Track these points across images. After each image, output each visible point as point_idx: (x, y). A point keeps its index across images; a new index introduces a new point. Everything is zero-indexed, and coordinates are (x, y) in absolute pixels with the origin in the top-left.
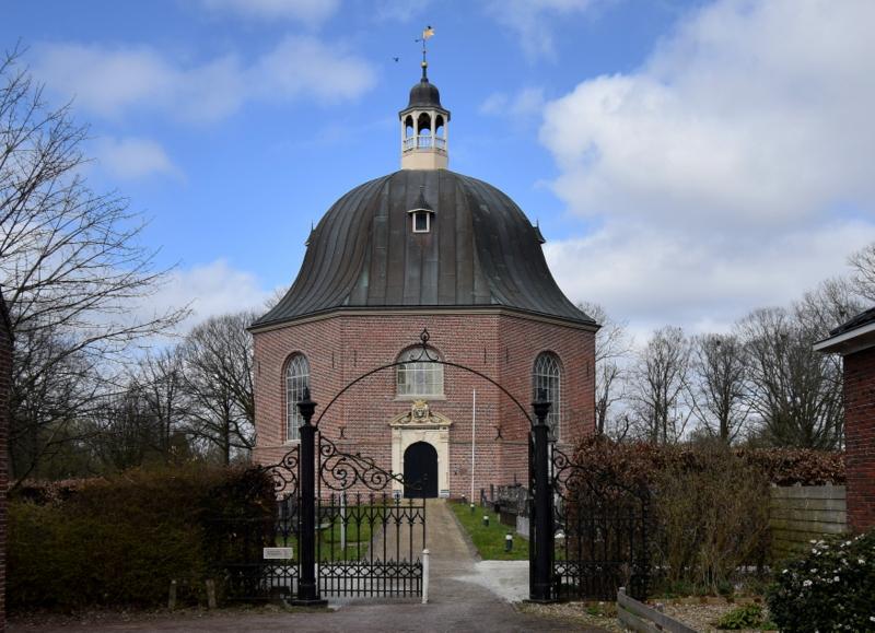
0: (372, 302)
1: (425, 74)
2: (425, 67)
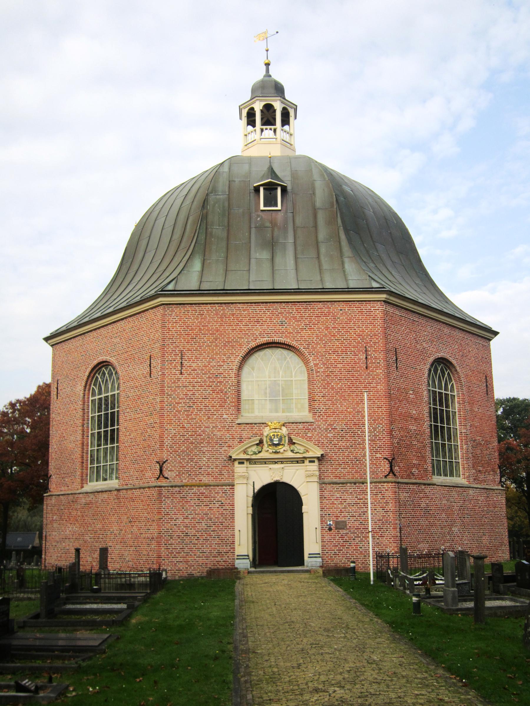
1: (268, 70)
2: (267, 65)
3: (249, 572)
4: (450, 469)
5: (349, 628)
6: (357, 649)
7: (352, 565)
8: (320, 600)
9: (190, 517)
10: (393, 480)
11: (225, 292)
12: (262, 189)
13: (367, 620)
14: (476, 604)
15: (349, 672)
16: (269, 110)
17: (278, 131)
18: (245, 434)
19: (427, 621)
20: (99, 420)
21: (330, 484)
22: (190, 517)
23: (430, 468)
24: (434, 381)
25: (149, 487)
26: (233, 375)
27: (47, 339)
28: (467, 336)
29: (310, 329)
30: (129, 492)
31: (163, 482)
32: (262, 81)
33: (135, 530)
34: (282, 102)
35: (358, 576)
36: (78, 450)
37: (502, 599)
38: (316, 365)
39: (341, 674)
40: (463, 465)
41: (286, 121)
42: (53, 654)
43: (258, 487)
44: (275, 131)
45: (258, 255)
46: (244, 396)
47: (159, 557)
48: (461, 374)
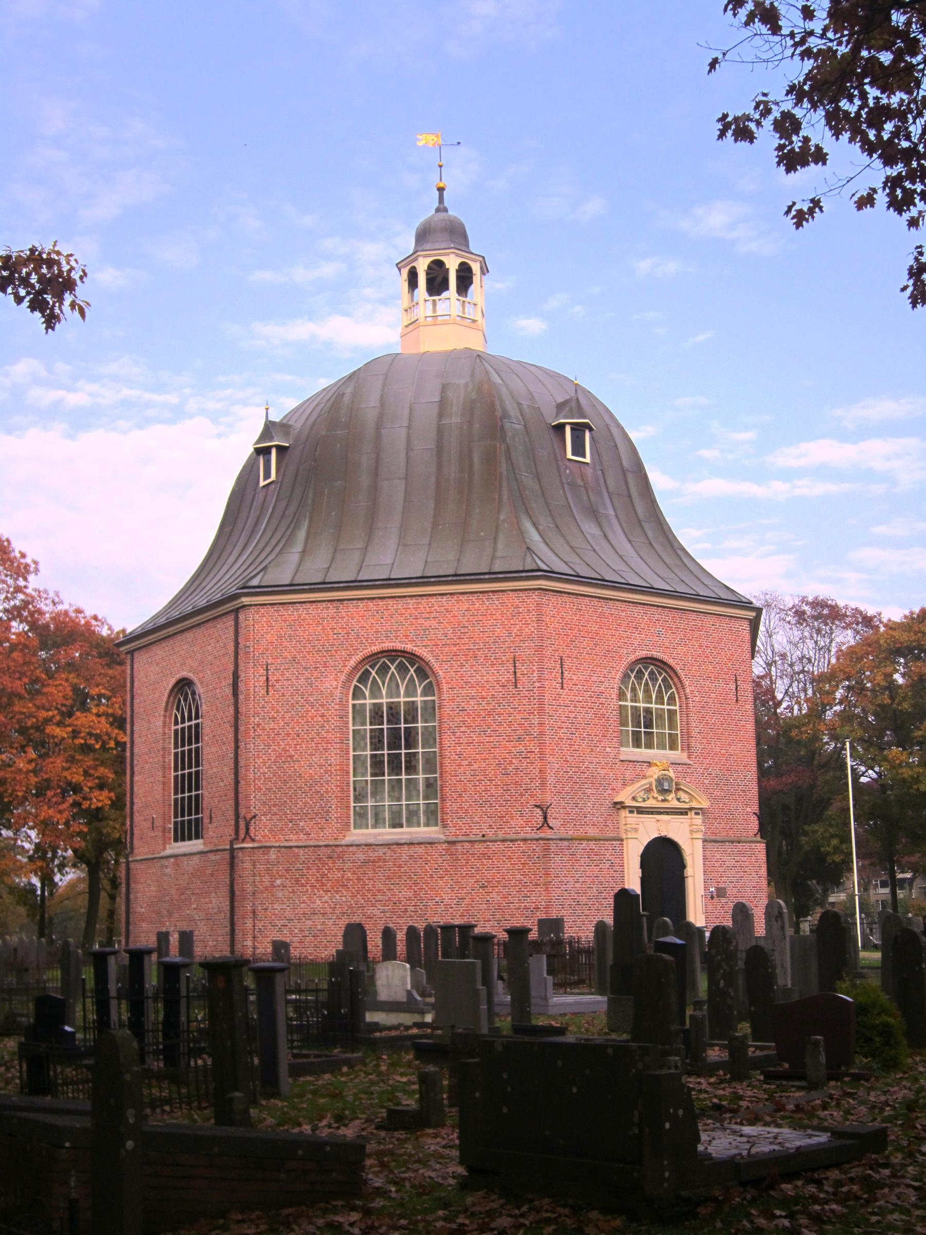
22: (581, 880)
31: (548, 834)
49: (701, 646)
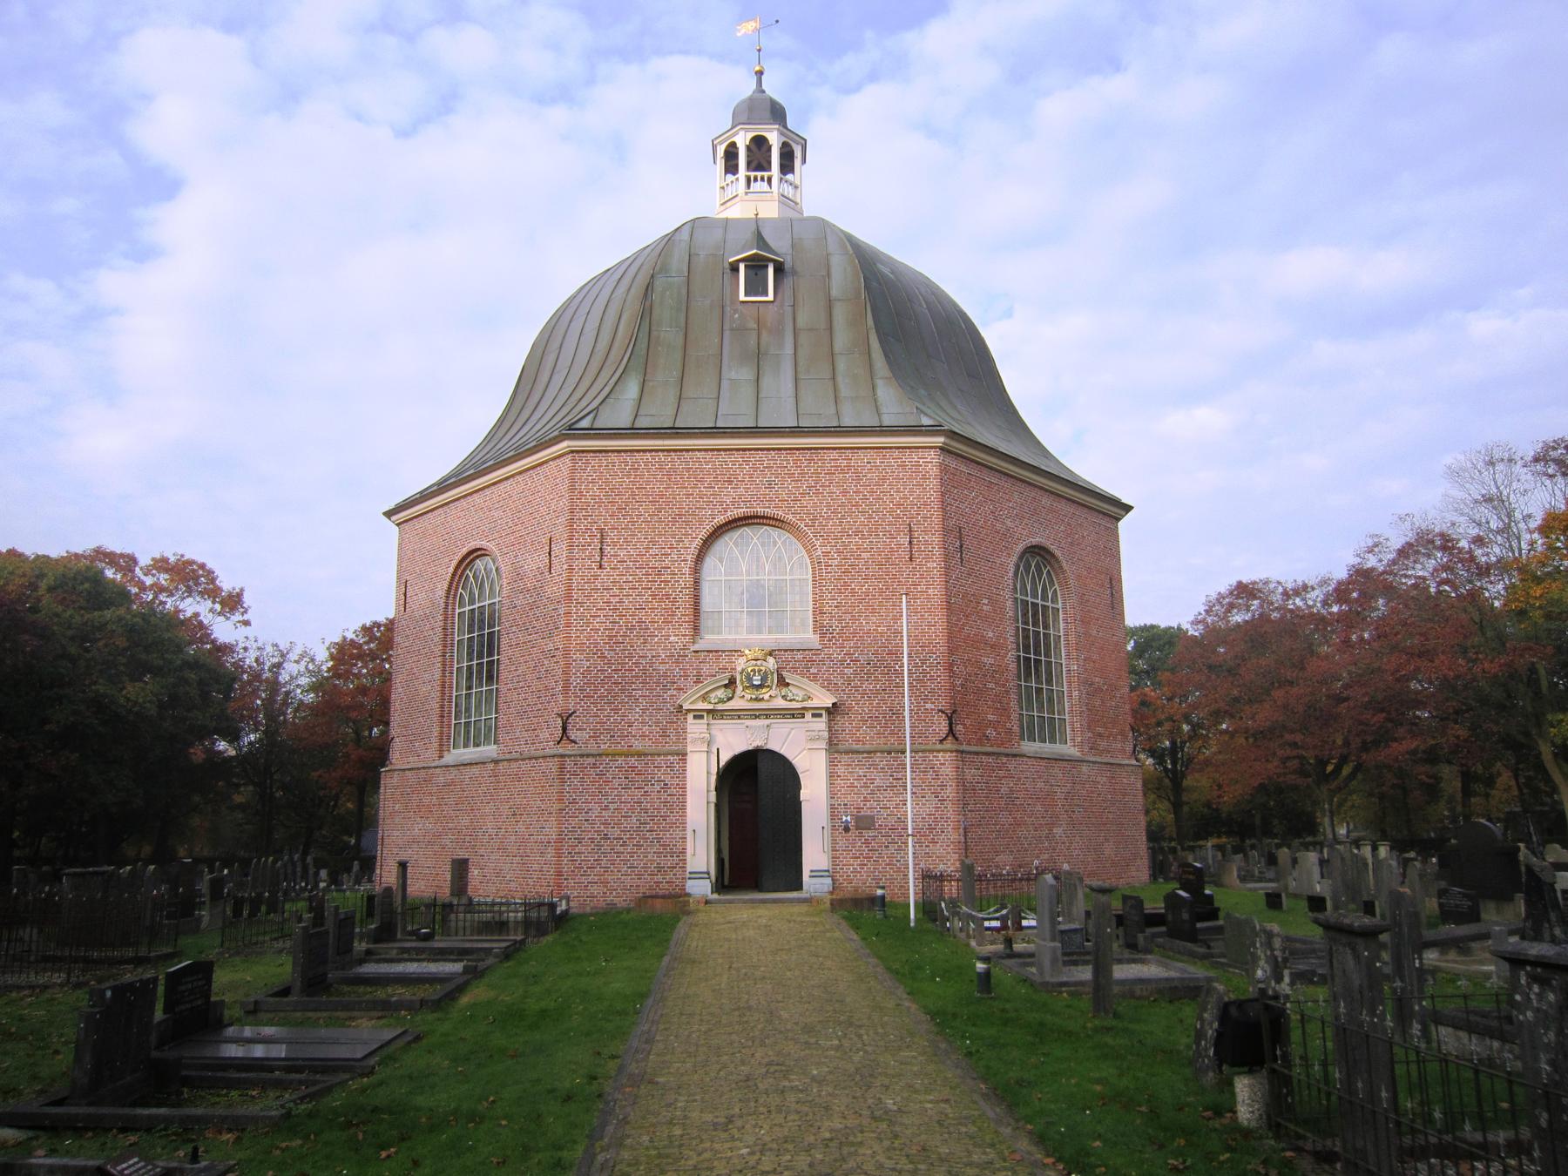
0: (643, 422)
1: (759, 83)
2: (760, 73)
3: (707, 902)
4: (1050, 731)
5: (851, 1024)
6: (858, 1078)
7: (880, 892)
8: (813, 959)
9: (611, 807)
10: (955, 747)
11: (675, 432)
12: (742, 267)
13: (891, 1004)
14: (1096, 972)
15: (826, 1143)
16: (765, 149)
17: (775, 181)
18: (705, 669)
19: (1003, 1010)
20: (470, 647)
21: (847, 752)
22: (611, 807)
23: (1016, 729)
24: (1024, 586)
25: (544, 757)
26: (686, 570)
27: (389, 514)
28: (1084, 513)
29: (817, 493)
30: (514, 765)
31: (568, 749)
32: (751, 99)
33: (521, 828)
34: (782, 134)
35: (889, 912)
36: (436, 694)
37: (1143, 962)
38: (826, 554)
39: (809, 1149)
40: (1072, 724)
41: (787, 166)
42: (269, 1075)
43: (725, 757)
44: (770, 179)
45: (733, 375)
46: (707, 604)
47: (559, 874)
48: (1069, 574)
49: (845, 493)
